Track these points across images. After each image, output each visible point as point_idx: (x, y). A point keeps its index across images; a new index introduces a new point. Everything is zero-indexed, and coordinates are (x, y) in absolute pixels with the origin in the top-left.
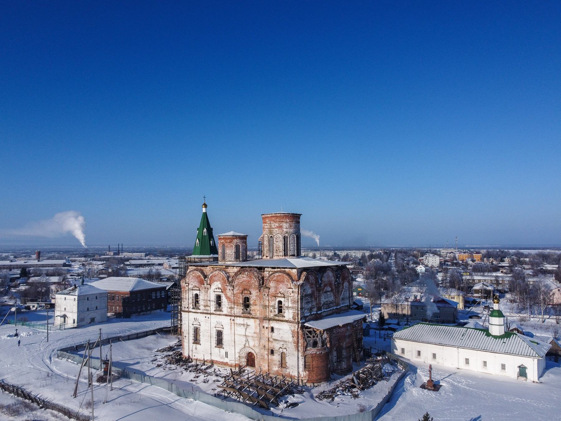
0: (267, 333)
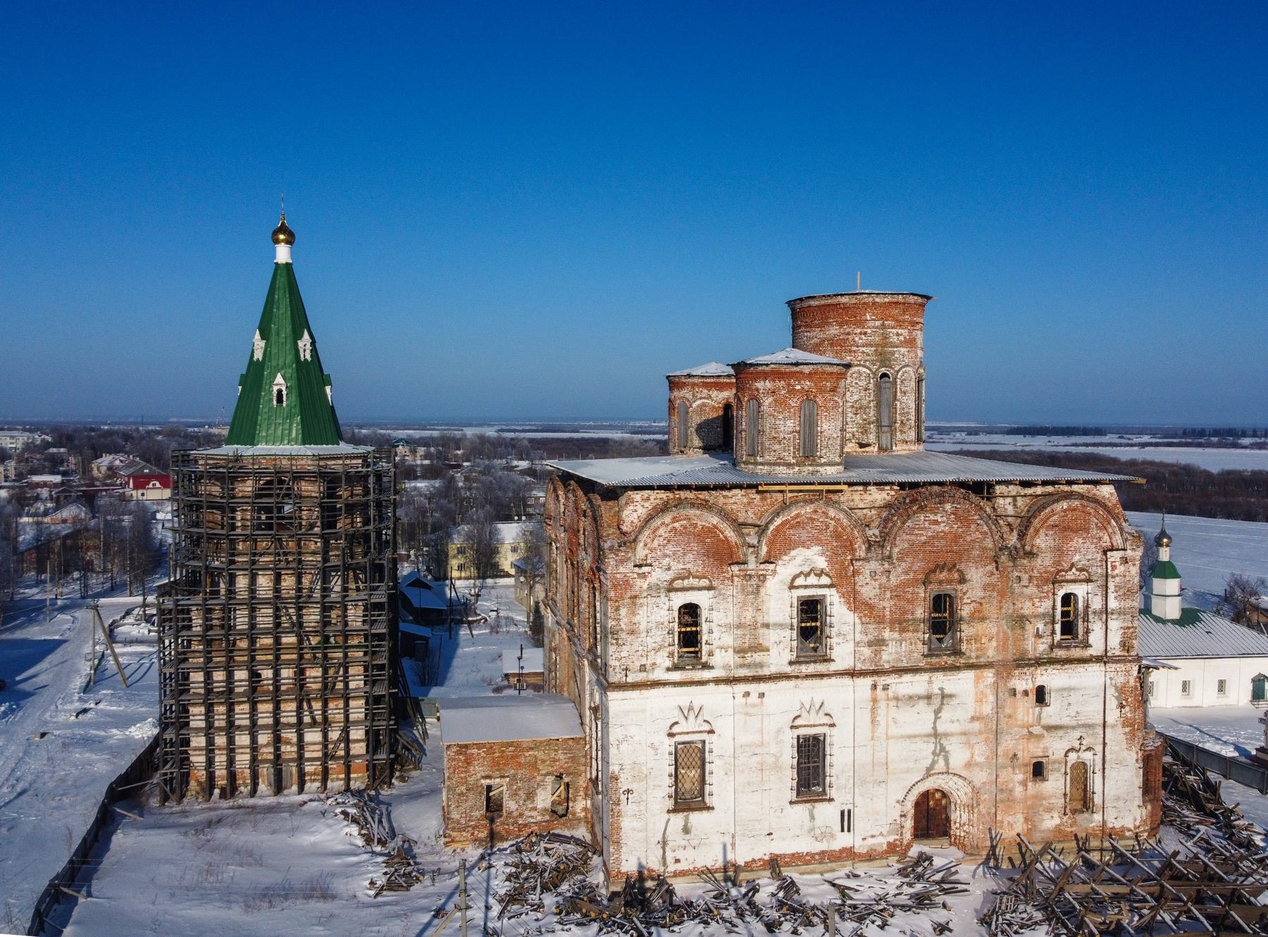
0: (1025, 710)
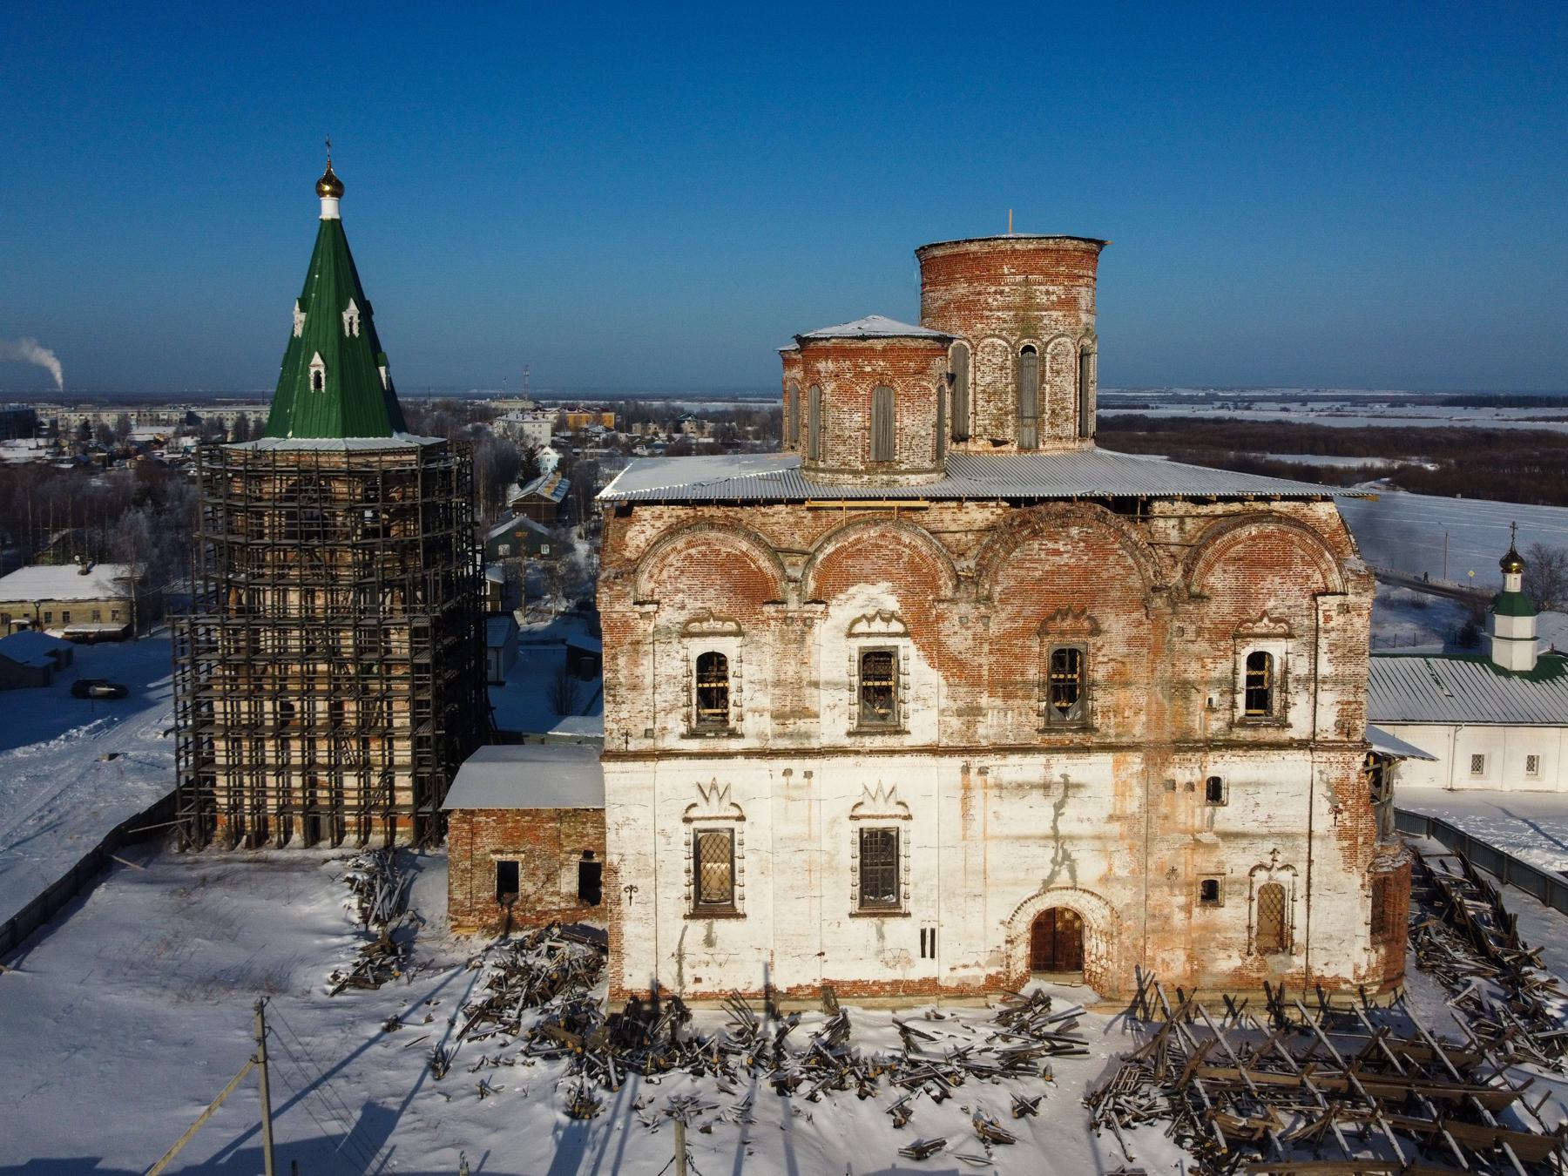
0: (1191, 811)
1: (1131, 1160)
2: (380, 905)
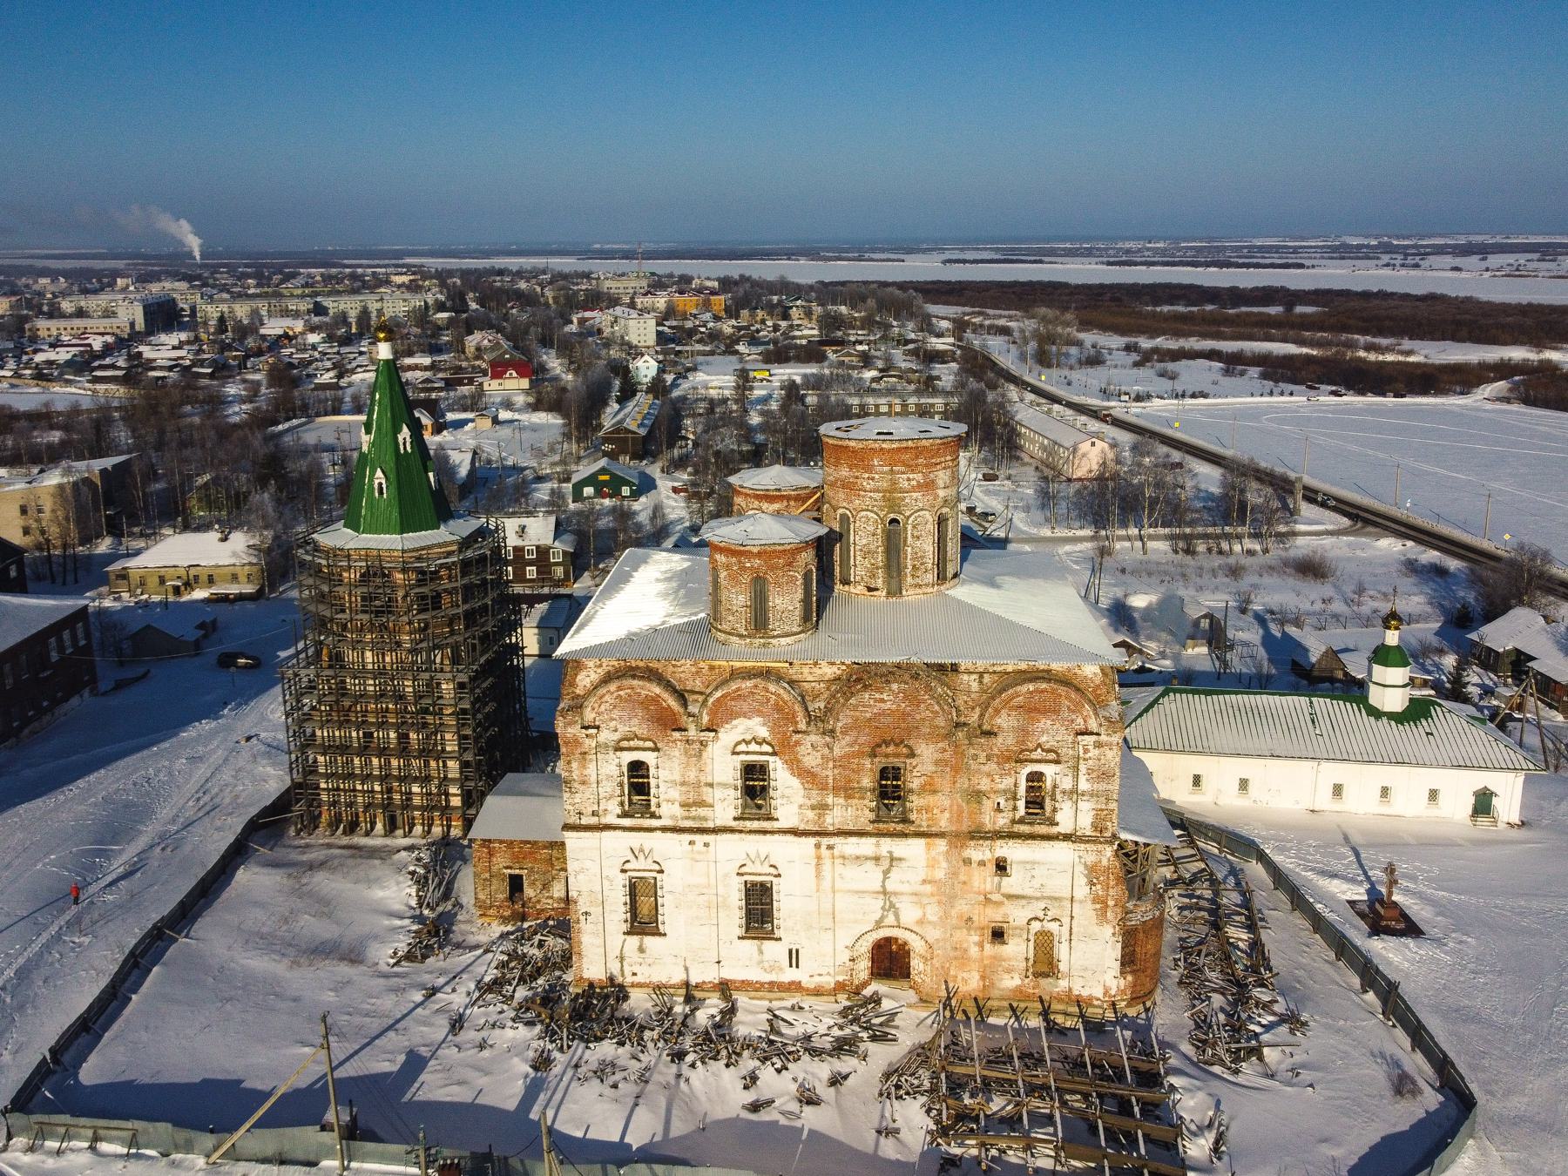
0: (984, 879)
1: (894, 1121)
2: (432, 894)
